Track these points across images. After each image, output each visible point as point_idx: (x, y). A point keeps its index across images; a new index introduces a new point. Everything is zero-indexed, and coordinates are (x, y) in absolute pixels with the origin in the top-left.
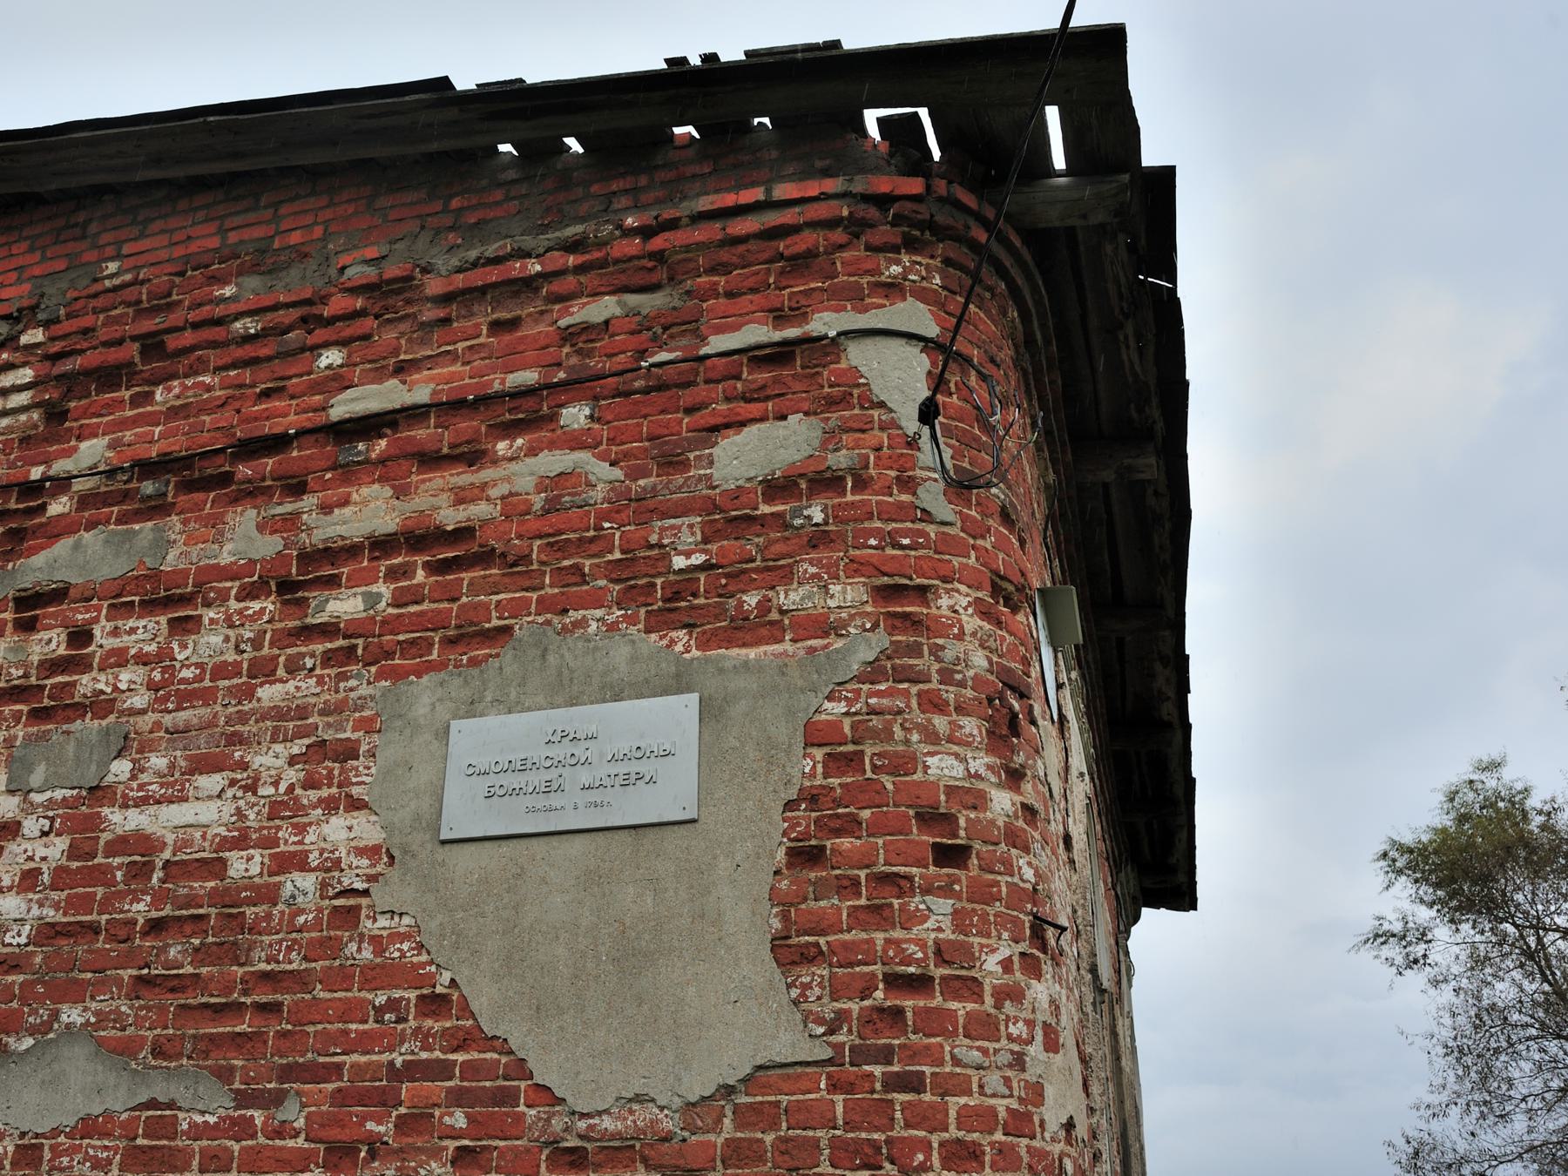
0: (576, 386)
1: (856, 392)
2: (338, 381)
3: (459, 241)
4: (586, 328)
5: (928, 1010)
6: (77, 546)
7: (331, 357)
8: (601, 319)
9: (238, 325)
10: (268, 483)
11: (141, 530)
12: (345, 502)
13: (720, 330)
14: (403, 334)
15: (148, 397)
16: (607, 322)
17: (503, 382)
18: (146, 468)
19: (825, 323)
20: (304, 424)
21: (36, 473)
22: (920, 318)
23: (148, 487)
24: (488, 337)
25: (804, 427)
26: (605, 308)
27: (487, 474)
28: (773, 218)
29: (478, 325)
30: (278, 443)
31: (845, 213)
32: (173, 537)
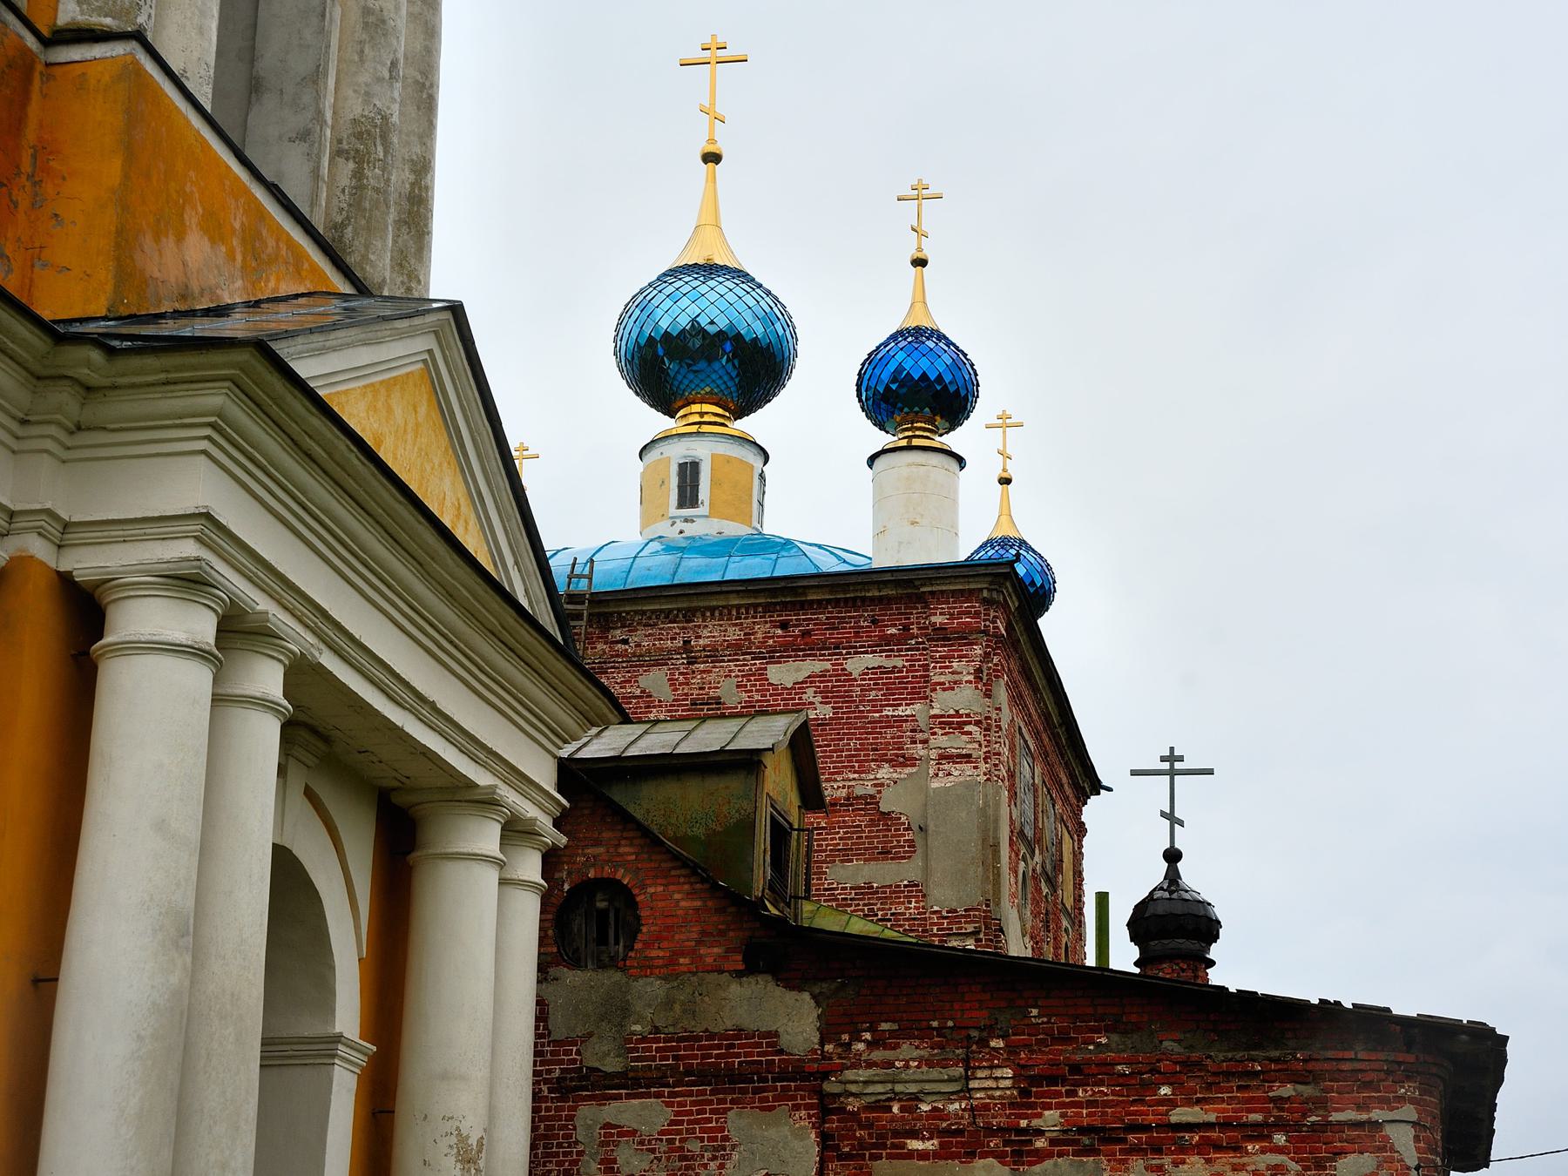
0: (1280, 1126)
1: (1388, 1145)
2: (1171, 1103)
3: (1216, 1038)
4: (1281, 1099)
5: (680, 1135)
6: (1056, 1165)
7: (1165, 1090)
8: (1286, 1096)
9: (1119, 1067)
10: (1145, 1146)
11: (1087, 1162)
12: (1184, 1162)
13: (1337, 1110)
14: (1197, 1084)
15: (1073, 1093)
16: (1289, 1097)
17: (1247, 1118)
18: (1083, 1130)
19: (1377, 1115)
20: (51, 384)
21: (1024, 1123)
22: (1409, 1112)
23: (1086, 1140)
24: (1237, 1092)
25: (1370, 1159)
26: (1288, 1090)
27: (1245, 1160)
28: (1357, 1066)
29: (1232, 1087)
30: (1146, 1128)
31: (1385, 1068)
32: (1104, 1167)
